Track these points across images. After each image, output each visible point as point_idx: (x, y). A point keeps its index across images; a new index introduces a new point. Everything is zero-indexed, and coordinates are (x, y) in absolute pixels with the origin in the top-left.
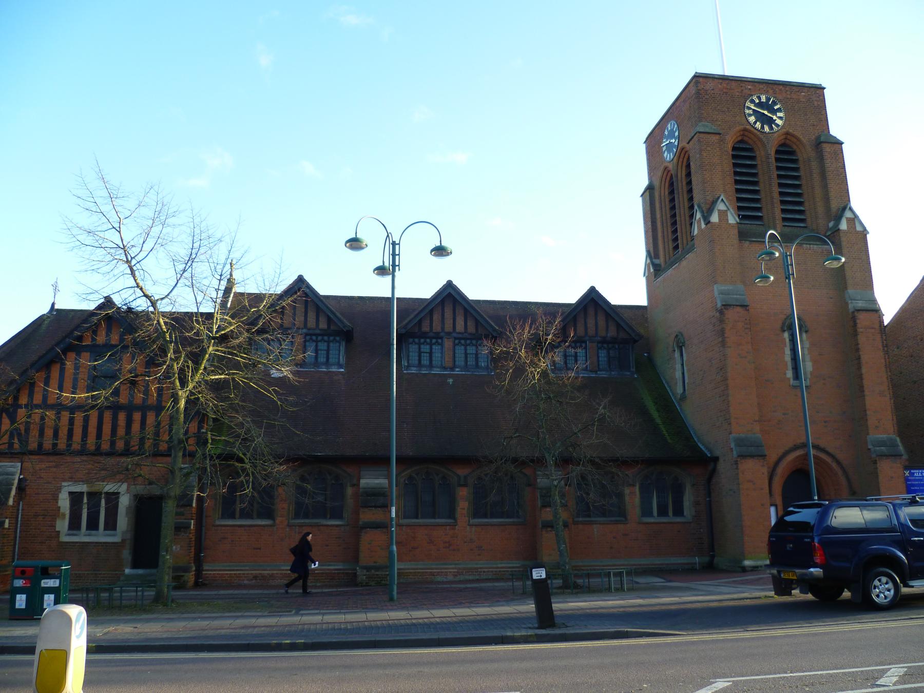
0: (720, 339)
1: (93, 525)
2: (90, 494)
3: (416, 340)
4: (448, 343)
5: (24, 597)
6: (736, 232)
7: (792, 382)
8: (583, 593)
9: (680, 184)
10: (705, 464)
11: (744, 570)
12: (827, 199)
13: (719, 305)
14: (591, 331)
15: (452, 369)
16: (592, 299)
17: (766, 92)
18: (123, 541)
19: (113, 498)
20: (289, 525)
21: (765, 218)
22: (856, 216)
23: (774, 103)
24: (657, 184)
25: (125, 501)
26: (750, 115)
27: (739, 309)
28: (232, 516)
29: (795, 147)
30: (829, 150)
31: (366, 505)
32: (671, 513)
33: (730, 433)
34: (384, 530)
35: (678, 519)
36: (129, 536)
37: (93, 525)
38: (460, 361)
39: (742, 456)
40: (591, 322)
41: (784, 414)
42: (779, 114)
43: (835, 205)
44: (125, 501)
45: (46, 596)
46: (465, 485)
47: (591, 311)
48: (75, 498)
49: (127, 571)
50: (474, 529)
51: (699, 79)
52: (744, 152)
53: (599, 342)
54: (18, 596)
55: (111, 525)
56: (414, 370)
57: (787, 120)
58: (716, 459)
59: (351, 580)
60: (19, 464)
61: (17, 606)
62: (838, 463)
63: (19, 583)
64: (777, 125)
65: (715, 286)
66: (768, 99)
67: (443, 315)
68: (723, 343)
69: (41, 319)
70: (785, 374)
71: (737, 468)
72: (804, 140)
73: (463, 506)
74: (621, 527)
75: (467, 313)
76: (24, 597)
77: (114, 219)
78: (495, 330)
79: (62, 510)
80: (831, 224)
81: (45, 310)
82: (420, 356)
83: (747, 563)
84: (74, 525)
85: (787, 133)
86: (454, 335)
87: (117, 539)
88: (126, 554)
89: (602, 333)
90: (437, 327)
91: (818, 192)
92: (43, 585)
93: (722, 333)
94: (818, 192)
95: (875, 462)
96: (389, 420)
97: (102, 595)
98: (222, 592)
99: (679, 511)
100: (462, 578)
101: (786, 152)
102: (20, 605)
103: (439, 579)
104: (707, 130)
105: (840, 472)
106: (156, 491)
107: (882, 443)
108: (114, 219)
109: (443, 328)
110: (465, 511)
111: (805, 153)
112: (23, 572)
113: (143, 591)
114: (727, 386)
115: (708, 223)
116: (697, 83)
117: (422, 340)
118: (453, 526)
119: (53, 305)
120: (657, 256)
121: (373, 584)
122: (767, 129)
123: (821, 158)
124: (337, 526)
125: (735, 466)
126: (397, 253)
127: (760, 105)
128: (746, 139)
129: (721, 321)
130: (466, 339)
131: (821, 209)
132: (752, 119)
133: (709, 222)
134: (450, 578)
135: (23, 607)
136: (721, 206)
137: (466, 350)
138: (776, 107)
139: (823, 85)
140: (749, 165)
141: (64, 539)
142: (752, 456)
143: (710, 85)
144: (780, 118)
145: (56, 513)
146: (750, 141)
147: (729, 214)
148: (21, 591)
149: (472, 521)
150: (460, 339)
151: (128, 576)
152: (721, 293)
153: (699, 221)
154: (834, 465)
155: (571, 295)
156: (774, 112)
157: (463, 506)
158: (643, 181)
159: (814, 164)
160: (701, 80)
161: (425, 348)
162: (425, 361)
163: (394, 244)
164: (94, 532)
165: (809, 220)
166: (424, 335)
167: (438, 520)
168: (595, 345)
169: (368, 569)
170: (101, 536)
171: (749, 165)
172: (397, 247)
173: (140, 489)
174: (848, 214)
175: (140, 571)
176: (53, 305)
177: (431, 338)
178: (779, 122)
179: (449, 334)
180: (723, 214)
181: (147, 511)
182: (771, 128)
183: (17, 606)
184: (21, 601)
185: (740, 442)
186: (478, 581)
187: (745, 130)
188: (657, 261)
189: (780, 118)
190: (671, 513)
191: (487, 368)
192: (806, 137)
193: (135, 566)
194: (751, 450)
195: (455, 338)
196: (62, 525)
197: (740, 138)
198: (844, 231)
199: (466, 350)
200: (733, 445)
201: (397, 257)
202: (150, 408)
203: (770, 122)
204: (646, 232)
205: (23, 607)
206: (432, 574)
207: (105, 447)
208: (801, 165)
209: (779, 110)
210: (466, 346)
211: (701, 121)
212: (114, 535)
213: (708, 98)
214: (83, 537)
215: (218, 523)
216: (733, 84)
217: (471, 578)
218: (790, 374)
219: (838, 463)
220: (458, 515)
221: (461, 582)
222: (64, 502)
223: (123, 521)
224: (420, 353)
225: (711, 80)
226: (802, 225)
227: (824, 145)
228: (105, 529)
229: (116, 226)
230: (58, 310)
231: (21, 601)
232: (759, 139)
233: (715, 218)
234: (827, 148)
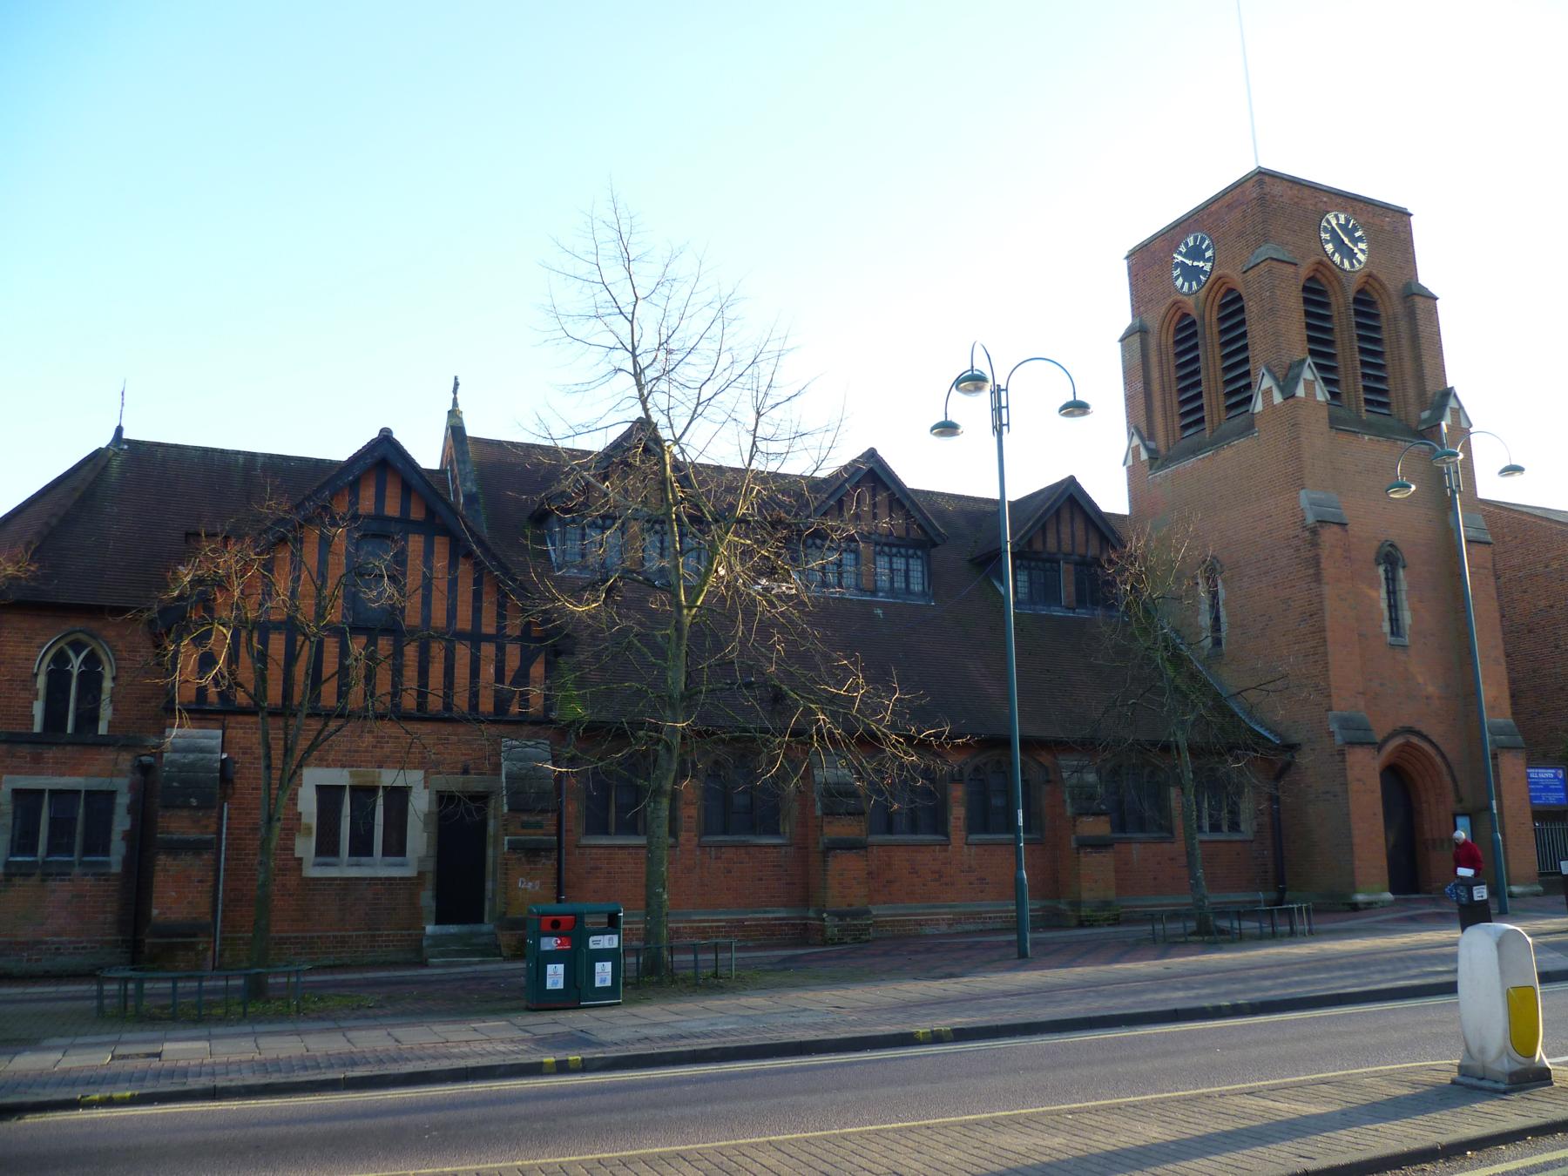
0: (1312, 571)
1: (361, 846)
2: (354, 789)
5: (560, 968)
6: (1324, 414)
7: (1389, 639)
8: (1232, 941)
9: (1208, 331)
10: (1280, 758)
11: (1355, 907)
12: (1420, 377)
13: (1310, 520)
14: (1066, 547)
17: (1344, 210)
18: (421, 874)
19: (398, 797)
20: (700, 846)
21: (1344, 396)
22: (1461, 407)
23: (1355, 229)
24: (1153, 323)
25: (420, 803)
26: (1327, 242)
27: (1336, 528)
28: (605, 831)
29: (1376, 296)
30: (1418, 304)
31: (830, 812)
32: (1225, 828)
33: (1330, 709)
34: (862, 852)
35: (1236, 837)
36: (430, 866)
37: (361, 846)
38: (883, 581)
39: (1351, 744)
40: (1065, 530)
42: (1362, 246)
43: (1431, 387)
44: (420, 803)
45: (598, 966)
46: (960, 781)
47: (1065, 515)
48: (328, 796)
49: (430, 929)
50: (974, 850)
51: (1262, 177)
52: (1316, 292)
53: (1076, 564)
54: (550, 968)
55: (395, 845)
57: (1371, 253)
58: (1292, 748)
59: (803, 934)
60: (220, 732)
61: (549, 986)
62: (1443, 756)
63: (549, 944)
64: (1359, 262)
65: (1302, 493)
68: (1317, 578)
69: (96, 455)
71: (1343, 761)
72: (1390, 286)
73: (957, 814)
74: (1166, 846)
75: (407, 490)
76: (560, 968)
77: (625, 299)
78: (939, 534)
79: (304, 820)
80: (1425, 415)
81: (104, 440)
83: (1360, 897)
84: (327, 847)
85: (1370, 275)
87: (409, 872)
88: (427, 899)
89: (1081, 550)
91: (1408, 365)
92: (592, 946)
93: (1316, 562)
94: (1408, 365)
95: (1342, 753)
97: (106, 987)
98: (370, 975)
99: (1234, 826)
100: (959, 928)
101: (1365, 303)
102: (555, 983)
103: (927, 930)
104: (1280, 257)
105: (1444, 769)
106: (476, 783)
108: (625, 299)
110: (961, 823)
111: (1389, 308)
112: (556, 925)
113: (140, 982)
114: (1325, 640)
115: (1289, 395)
116: (1261, 183)
118: (945, 845)
119: (119, 430)
120: (1152, 436)
121: (848, 940)
122: (1347, 265)
123: (1412, 315)
124: (775, 846)
125: (1338, 758)
126: (1004, 404)
127: (1343, 227)
128: (1319, 276)
129: (1314, 544)
130: (890, 545)
131: (1411, 393)
132: (1329, 247)
133: (1293, 396)
134: (944, 928)
135: (561, 986)
136: (1308, 374)
137: (891, 563)
139: (1410, 210)
140: (1286, 312)
141: (311, 872)
142: (1361, 744)
143: (1278, 189)
144: (1362, 251)
145: (294, 825)
146: (1324, 281)
148: (554, 957)
149: (974, 838)
151: (433, 937)
152: (1313, 503)
153: (1269, 392)
154: (1438, 759)
156: (1355, 241)
157: (957, 814)
158: (1122, 317)
159: (1403, 325)
160: (1267, 179)
163: (999, 390)
164: (364, 859)
165: (1394, 405)
167: (920, 837)
168: (1071, 567)
169: (841, 915)
170: (378, 867)
171: (1286, 312)
172: (1003, 394)
173: (454, 783)
174: (1452, 403)
175: (453, 929)
176: (119, 430)
180: (1309, 385)
181: (460, 824)
182: (1352, 265)
183: (549, 986)
184: (555, 976)
185: (1346, 723)
186: (982, 932)
187: (1320, 263)
188: (1152, 445)
189: (1362, 251)
190: (1225, 828)
191: (923, 594)
192: (1393, 284)
193: (438, 922)
194: (1359, 737)
196: (305, 847)
199: (891, 563)
200: (1334, 727)
201: (1004, 411)
202: (461, 636)
203: (1351, 255)
204: (1130, 399)
205: (561, 986)
206: (919, 923)
207: (435, 703)
208: (1383, 322)
209: (1360, 239)
210: (891, 556)
211: (1266, 241)
212: (402, 865)
213: (1266, 207)
214: (345, 868)
215: (584, 842)
216: (1307, 192)
217: (972, 927)
218: (1386, 627)
219: (1443, 756)
220: (950, 829)
221: (958, 934)
222: (307, 803)
223: (418, 839)
227: (1417, 299)
228: (385, 854)
229: (628, 310)
230: (128, 441)
231: (555, 976)
232: (1337, 278)
233: (1300, 392)
234: (1420, 303)
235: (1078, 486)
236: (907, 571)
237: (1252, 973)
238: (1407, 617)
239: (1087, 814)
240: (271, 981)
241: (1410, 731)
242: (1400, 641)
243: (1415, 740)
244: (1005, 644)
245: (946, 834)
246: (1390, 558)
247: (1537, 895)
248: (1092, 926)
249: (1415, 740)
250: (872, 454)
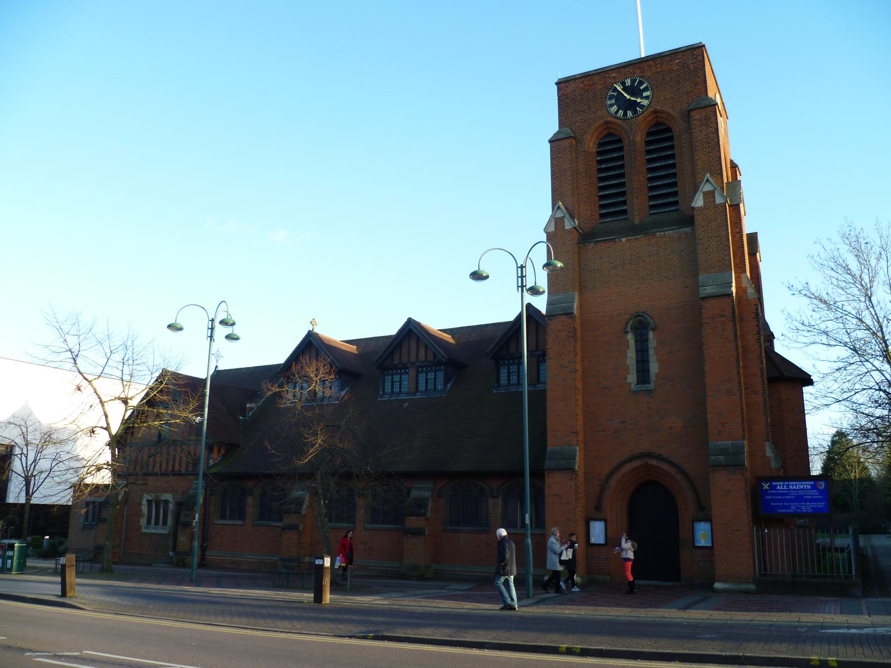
1: (157, 523)
3: (506, 362)
4: (412, 372)
15: (415, 394)
16: (311, 345)
27: (564, 318)
41: (622, 422)
55: (165, 523)
56: (386, 398)
66: (633, 81)
67: (409, 348)
70: (626, 379)
73: (361, 513)
82: (509, 376)
83: (717, 585)
84: (149, 522)
85: (655, 112)
86: (418, 364)
90: (396, 361)
96: (522, 434)
107: (724, 451)
109: (409, 360)
117: (511, 361)
130: (427, 367)
138: (642, 88)
141: (144, 531)
145: (140, 514)
147: (566, 220)
150: (422, 367)
154: (679, 477)
155: (391, 328)
161: (397, 378)
162: (396, 390)
166: (395, 367)
177: (401, 369)
178: (645, 102)
179: (413, 363)
187: (607, 123)
195: (419, 367)
196: (143, 522)
197: (606, 132)
198: (699, 209)
199: (427, 376)
218: (632, 378)
224: (393, 382)
225: (572, 82)
226: (673, 208)
235: (418, 325)
236: (400, 382)
237: (295, 613)
238: (654, 367)
239: (413, 515)
240: (752, 587)
241: (650, 455)
242: (645, 387)
243: (654, 462)
244: (521, 412)
245: (354, 523)
246: (641, 327)
247: (746, 592)
248: (406, 579)
249: (654, 462)
250: (410, 321)
